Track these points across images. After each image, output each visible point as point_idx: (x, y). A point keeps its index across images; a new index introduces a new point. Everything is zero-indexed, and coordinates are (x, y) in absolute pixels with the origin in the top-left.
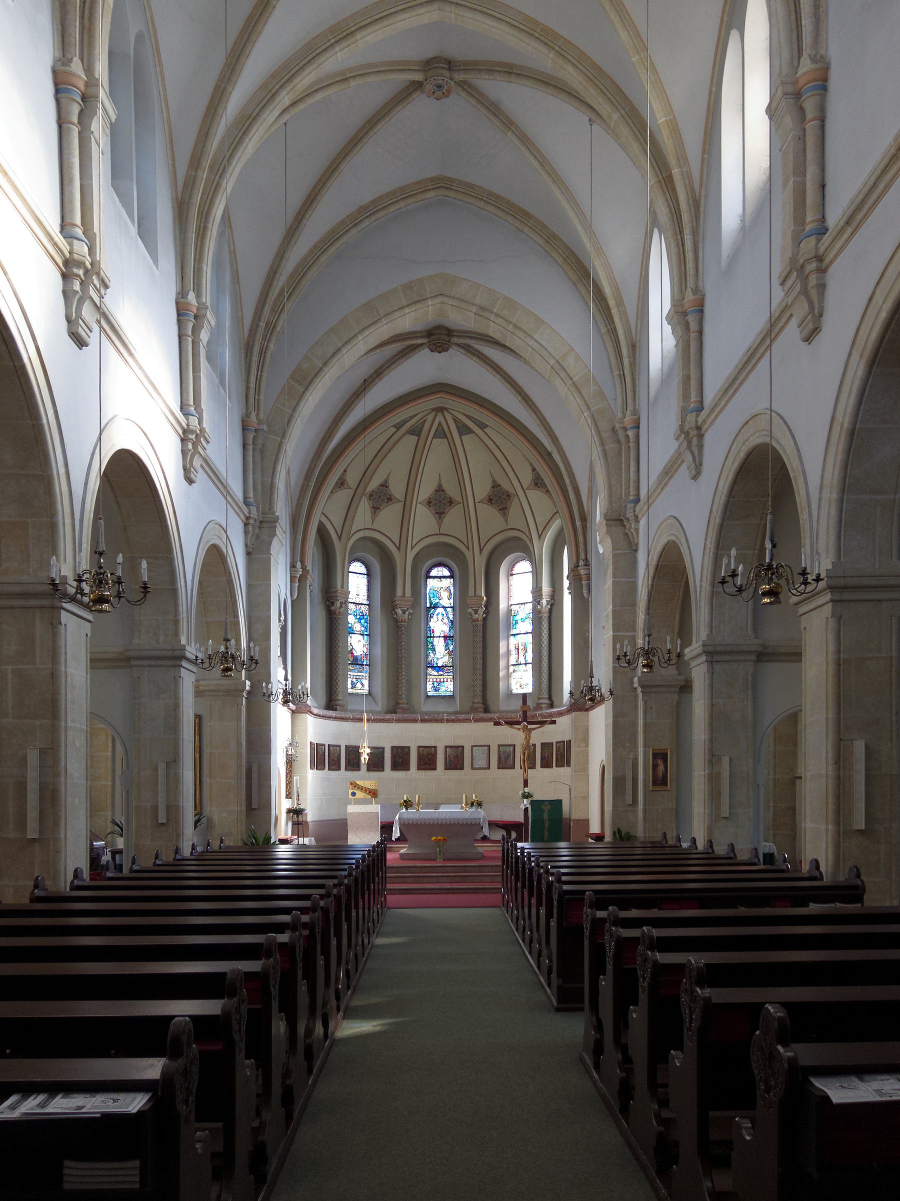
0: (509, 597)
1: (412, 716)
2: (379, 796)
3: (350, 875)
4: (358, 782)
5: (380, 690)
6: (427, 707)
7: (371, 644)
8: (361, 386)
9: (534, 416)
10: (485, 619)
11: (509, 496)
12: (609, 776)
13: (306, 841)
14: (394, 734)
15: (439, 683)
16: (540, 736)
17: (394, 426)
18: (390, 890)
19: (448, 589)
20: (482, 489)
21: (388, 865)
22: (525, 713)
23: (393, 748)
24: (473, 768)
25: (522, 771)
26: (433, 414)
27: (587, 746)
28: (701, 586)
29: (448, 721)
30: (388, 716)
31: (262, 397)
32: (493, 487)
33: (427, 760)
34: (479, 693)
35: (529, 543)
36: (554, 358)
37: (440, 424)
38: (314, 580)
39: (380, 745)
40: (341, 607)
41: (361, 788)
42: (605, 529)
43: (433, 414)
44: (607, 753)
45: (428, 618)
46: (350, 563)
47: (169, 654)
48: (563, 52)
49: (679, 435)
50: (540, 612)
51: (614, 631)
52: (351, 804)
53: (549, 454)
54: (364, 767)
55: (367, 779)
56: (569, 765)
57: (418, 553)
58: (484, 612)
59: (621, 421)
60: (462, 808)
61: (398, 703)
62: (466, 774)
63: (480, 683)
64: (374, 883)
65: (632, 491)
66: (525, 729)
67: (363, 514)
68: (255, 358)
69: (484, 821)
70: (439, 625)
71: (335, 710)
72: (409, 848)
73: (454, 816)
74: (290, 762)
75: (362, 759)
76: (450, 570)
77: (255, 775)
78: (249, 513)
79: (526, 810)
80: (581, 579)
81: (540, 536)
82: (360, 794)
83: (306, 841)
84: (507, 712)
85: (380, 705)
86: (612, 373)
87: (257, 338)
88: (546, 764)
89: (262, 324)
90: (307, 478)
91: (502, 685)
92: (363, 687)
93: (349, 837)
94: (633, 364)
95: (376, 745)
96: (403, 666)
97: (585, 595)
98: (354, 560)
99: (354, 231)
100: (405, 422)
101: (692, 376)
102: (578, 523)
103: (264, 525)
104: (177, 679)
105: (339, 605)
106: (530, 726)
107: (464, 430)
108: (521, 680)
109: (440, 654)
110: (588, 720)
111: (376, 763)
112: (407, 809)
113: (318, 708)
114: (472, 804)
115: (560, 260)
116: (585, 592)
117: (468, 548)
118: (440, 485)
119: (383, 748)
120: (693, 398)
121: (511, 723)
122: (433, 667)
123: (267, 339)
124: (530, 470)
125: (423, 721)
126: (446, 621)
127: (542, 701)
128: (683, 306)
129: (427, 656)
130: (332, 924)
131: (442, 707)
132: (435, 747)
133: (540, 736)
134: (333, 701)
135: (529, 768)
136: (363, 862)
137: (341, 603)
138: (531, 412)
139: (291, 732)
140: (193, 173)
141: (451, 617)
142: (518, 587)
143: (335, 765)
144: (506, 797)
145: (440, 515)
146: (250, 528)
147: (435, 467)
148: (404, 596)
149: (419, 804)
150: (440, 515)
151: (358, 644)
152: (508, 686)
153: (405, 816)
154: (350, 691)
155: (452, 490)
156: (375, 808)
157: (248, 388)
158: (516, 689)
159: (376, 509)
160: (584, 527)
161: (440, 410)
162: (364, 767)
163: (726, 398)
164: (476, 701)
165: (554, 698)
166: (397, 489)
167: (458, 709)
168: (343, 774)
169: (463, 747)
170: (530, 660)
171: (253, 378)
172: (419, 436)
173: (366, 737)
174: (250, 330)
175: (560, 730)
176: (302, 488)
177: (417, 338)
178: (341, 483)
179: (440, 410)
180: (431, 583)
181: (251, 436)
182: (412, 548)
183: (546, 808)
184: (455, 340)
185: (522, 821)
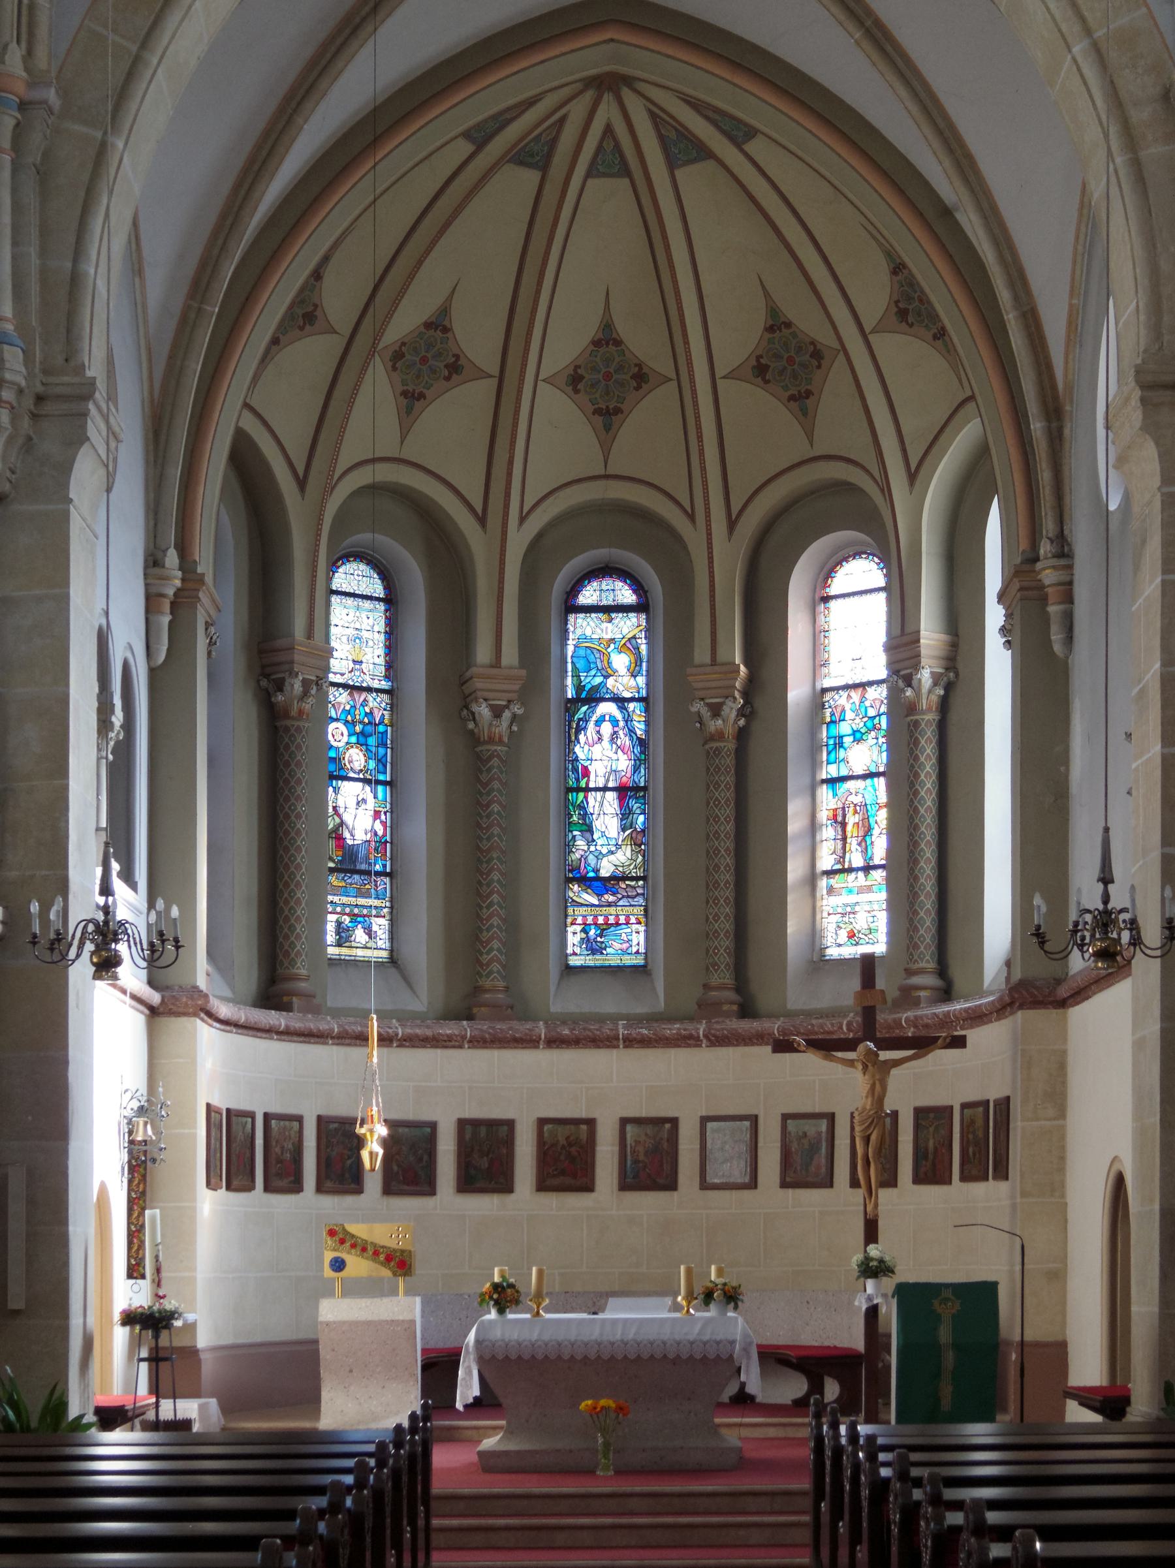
0: (818, 662)
1: (521, 1028)
3: (335, 1507)
4: (353, 1228)
5: (424, 949)
6: (566, 1002)
7: (397, 812)
9: (903, 92)
10: (742, 735)
11: (817, 355)
12: (1145, 1210)
13: (188, 1408)
14: (461, 1083)
15: (604, 929)
16: (918, 1083)
17: (467, 135)
19: (630, 645)
20: (736, 336)
21: (437, 1488)
22: (869, 1014)
23: (462, 1124)
24: (705, 1185)
25: (860, 1193)
26: (589, 95)
27: (1062, 1113)
29: (630, 1042)
30: (449, 1029)
32: (770, 329)
33: (566, 1160)
34: (724, 958)
37: (608, 130)
38: (222, 608)
39: (425, 1116)
40: (305, 694)
41: (362, 1247)
42: (1135, 416)
43: (589, 95)
44: (1140, 1133)
45: (571, 731)
46: (333, 566)
50: (912, 708)
52: (330, 1294)
53: (946, 213)
54: (373, 1182)
55: (377, 1217)
56: (1002, 1172)
57: (540, 536)
58: (741, 713)
60: (676, 1307)
61: (478, 990)
62: (685, 1202)
63: (729, 926)
64: (398, 1545)
66: (870, 1062)
69: (746, 1350)
70: (604, 755)
72: (510, 1432)
73: (651, 1334)
74: (141, 1166)
75: (365, 1154)
76: (638, 587)
79: (872, 1313)
80: (1044, 600)
81: (912, 477)
82: (358, 1266)
83: (188, 1408)
84: (809, 1014)
85: (423, 986)
88: (931, 1171)
90: (199, 286)
91: (794, 926)
92: (371, 942)
93: (325, 1395)
95: (410, 1115)
96: (495, 876)
97: (1058, 648)
98: (347, 557)
100: (501, 121)
102: (1037, 426)
105: (298, 687)
106: (885, 1055)
107: (682, 149)
108: (850, 916)
109: (608, 841)
110: (1063, 1035)
111: (410, 1167)
112: (501, 1311)
113: (234, 1001)
114: (708, 1297)
116: (1056, 637)
117: (692, 517)
118: (607, 326)
119: (433, 1126)
121: (826, 1046)
122: (584, 881)
124: (884, 268)
125: (555, 1042)
126: (624, 739)
127: (916, 980)
129: (567, 846)
130: (405, 1502)
131: (610, 1002)
132: (591, 1123)
133: (918, 1083)
134: (278, 981)
136: (381, 1464)
137: (306, 684)
138: (892, 77)
141: (640, 728)
142: (844, 631)
143: (284, 1177)
144: (813, 1272)
145: (607, 417)
147: (594, 274)
148: (497, 663)
149: (539, 1296)
150: (607, 417)
151: (357, 811)
152: (814, 934)
153: (497, 1334)
154: (332, 951)
155: (643, 341)
156: (403, 1307)
158: (839, 948)
159: (412, 400)
160: (1056, 439)
161: (609, 84)
164: (715, 980)
165: (957, 972)
166: (478, 339)
167: (661, 1005)
168: (311, 1204)
169: (674, 1121)
172: (544, 167)
173: (376, 1089)
175: (977, 1068)
176: (184, 320)
178: (305, 316)
179: (609, 84)
180: (583, 627)
182: (522, 519)
183: (947, 1310)
185: (859, 1344)
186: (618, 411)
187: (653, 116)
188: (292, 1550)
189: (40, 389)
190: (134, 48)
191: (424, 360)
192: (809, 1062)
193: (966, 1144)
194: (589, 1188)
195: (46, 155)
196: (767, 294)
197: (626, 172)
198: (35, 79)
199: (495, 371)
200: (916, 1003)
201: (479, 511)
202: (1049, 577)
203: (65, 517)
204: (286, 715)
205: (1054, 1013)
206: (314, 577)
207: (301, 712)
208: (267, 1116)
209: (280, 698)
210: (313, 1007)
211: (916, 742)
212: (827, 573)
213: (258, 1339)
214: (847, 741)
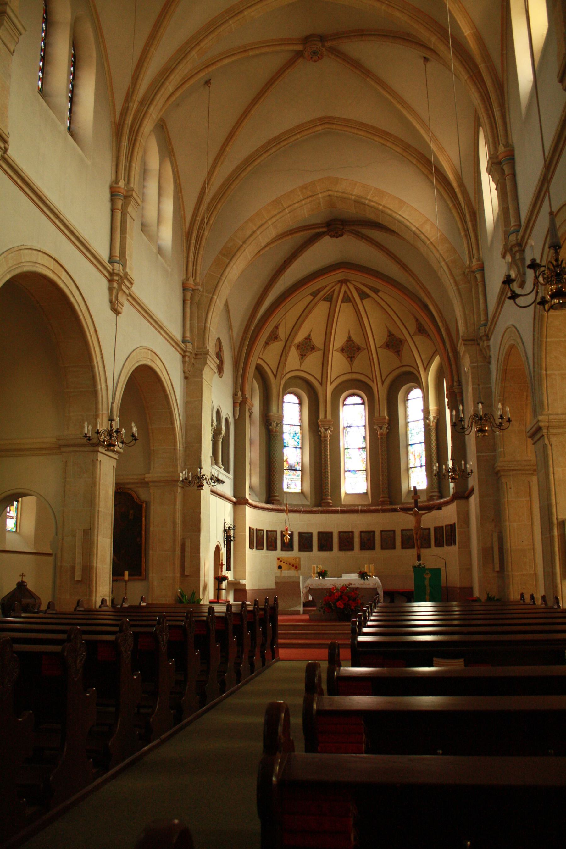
8: (282, 265)
11: (401, 341)
18: (282, 644)
26: (339, 285)
28: (534, 371)
31: (198, 267)
35: (417, 374)
36: (415, 226)
37: (345, 292)
39: (310, 531)
43: (339, 285)
48: (391, 4)
58: (387, 428)
59: (470, 267)
66: (416, 514)
68: (193, 241)
71: (272, 503)
77: (187, 549)
78: (186, 348)
87: (195, 228)
88: (439, 544)
89: (199, 219)
94: (475, 226)
99: (265, 156)
100: (319, 291)
101: (510, 207)
103: (199, 357)
105: (275, 425)
106: (420, 512)
107: (363, 296)
115: (414, 161)
117: (373, 381)
118: (350, 337)
119: (311, 534)
120: (513, 221)
124: (414, 320)
127: (434, 494)
128: (497, 158)
137: (277, 424)
139: (216, 515)
140: (127, 105)
142: (415, 408)
143: (272, 546)
148: (325, 417)
150: (351, 358)
155: (358, 340)
157: (187, 262)
159: (303, 356)
166: (318, 341)
168: (279, 553)
170: (424, 464)
171: (191, 254)
172: (331, 301)
173: (298, 523)
175: (448, 514)
177: (319, 228)
179: (343, 282)
181: (189, 295)
182: (331, 383)
183: (428, 576)
184: (348, 228)
186: (354, 357)
189: (196, 352)
190: (219, 276)
191: (305, 347)
193: (446, 536)
195: (199, 301)
196: (387, 328)
198: (196, 284)
199: (322, 348)
200: (433, 500)
201: (320, 381)
202: (456, 391)
203: (202, 381)
204: (272, 431)
206: (278, 399)
207: (276, 431)
208: (267, 531)
209: (270, 427)
210: (279, 503)
211: (430, 434)
213: (265, 588)
214: (415, 434)
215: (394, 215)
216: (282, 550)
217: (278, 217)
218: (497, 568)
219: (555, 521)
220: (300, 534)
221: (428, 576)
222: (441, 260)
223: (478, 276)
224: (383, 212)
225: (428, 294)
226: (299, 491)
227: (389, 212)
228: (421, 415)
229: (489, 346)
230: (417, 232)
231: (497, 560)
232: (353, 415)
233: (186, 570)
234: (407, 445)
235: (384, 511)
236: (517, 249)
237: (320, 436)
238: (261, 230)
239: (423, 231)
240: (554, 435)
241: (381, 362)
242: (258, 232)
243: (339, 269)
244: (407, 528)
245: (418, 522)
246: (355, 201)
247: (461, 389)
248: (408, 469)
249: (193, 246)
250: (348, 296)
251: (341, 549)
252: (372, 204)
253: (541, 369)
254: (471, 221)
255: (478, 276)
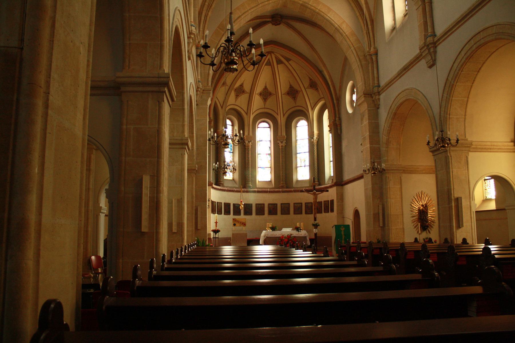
2: (247, 225)
35: (306, 112)
37: (269, 59)
47: (180, 142)
49: (423, 47)
50: (313, 142)
51: (370, 144)
54: (242, 212)
56: (332, 211)
59: (368, 52)
65: (376, 82)
67: (232, 99)
68: (203, 18)
71: (220, 186)
86: (362, 31)
88: (327, 211)
103: (205, 92)
104: (183, 156)
107: (279, 62)
117: (278, 114)
118: (266, 87)
120: (430, 30)
123: (208, 10)
135: (318, 213)
142: (301, 130)
143: (227, 212)
146: (199, 93)
147: (264, 79)
150: (265, 100)
155: (270, 89)
162: (242, 212)
163: (457, 26)
166: (247, 88)
168: (232, 216)
174: (201, 6)
177: (267, 18)
178: (224, 84)
183: (342, 229)
187: (276, 58)
188: (137, 287)
192: (306, 194)
194: (264, 214)
197: (270, 65)
202: (338, 123)
205: (341, 187)
212: (297, 122)
215: (325, 16)
216: (224, 214)
217: (255, 8)
218: (381, 225)
219: (453, 198)
220: (234, 205)
221: (342, 229)
222: (352, 46)
223: (374, 58)
224: (318, 13)
225: (324, 65)
226: (231, 178)
227: (322, 14)
228: (307, 136)
229: (379, 99)
230: (338, 27)
231: (381, 220)
232: (264, 135)
233: (198, 226)
234: (296, 153)
235: (283, 192)
236: (432, 45)
237: (245, 146)
238: (244, 15)
239: (342, 28)
240: (453, 151)
241: (285, 103)
242: (242, 17)
243: (271, 44)
244: (297, 202)
245: (316, 198)
246: (302, 5)
247: (341, 122)
248: (296, 168)
249: (202, 20)
250: (270, 62)
251: (257, 214)
252: (313, 8)
253: (447, 114)
254: (371, 25)
255: (374, 58)
